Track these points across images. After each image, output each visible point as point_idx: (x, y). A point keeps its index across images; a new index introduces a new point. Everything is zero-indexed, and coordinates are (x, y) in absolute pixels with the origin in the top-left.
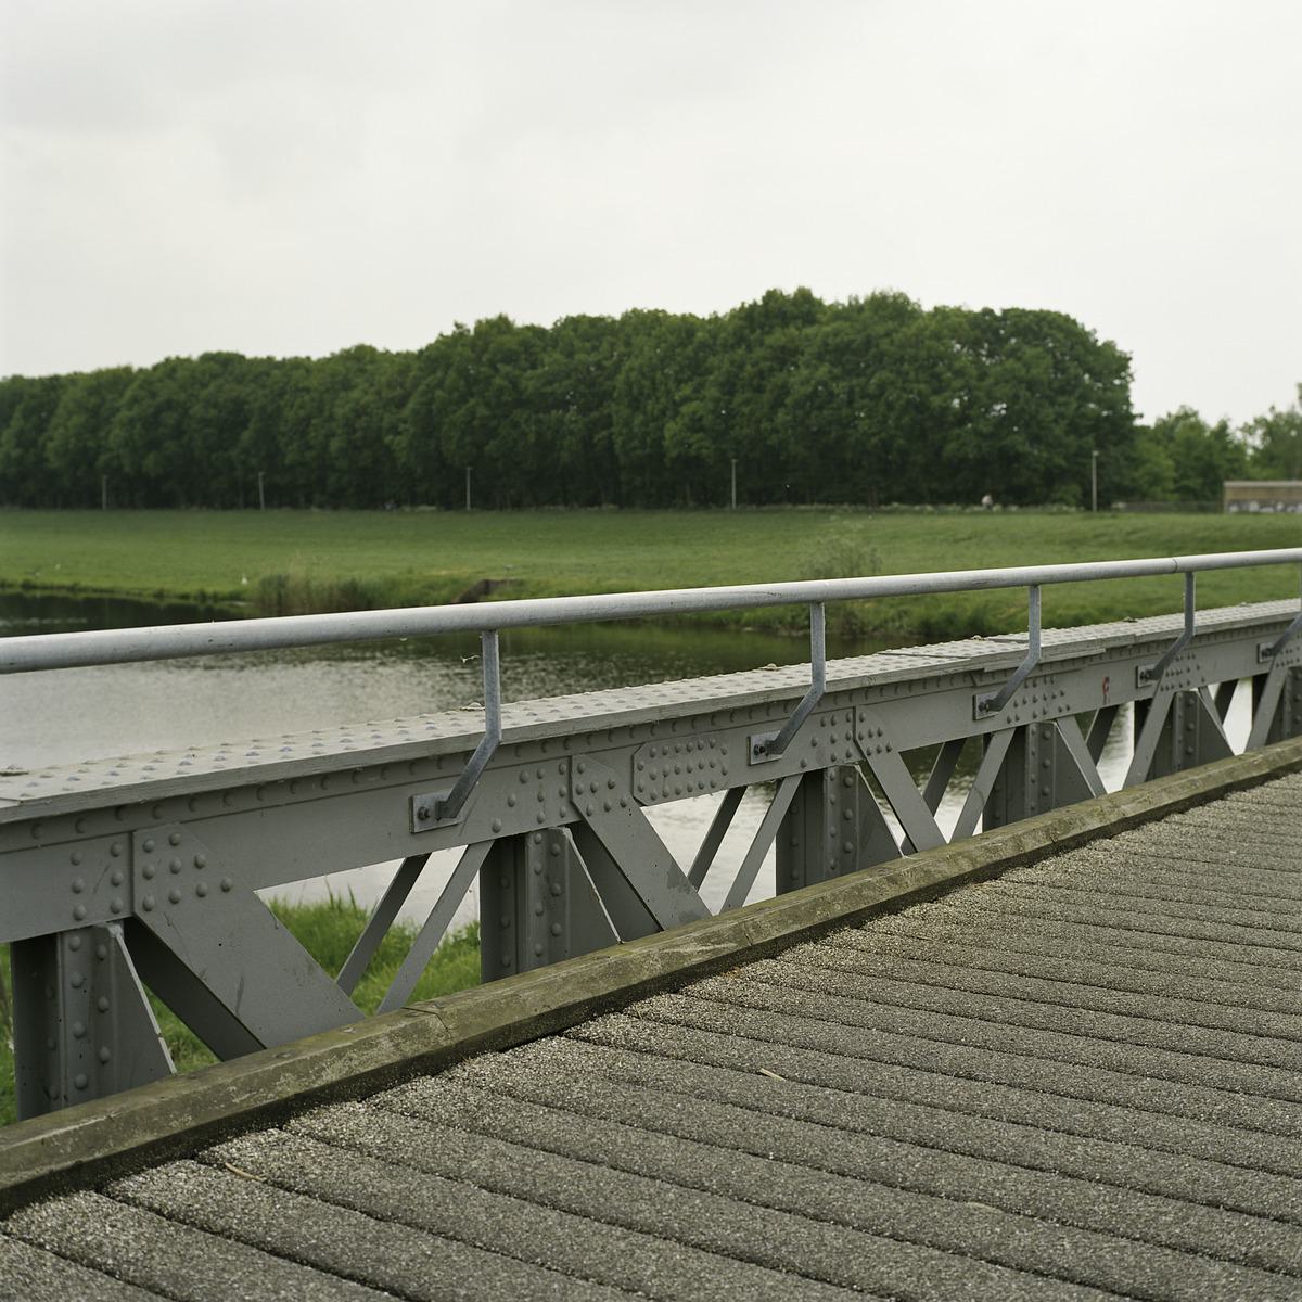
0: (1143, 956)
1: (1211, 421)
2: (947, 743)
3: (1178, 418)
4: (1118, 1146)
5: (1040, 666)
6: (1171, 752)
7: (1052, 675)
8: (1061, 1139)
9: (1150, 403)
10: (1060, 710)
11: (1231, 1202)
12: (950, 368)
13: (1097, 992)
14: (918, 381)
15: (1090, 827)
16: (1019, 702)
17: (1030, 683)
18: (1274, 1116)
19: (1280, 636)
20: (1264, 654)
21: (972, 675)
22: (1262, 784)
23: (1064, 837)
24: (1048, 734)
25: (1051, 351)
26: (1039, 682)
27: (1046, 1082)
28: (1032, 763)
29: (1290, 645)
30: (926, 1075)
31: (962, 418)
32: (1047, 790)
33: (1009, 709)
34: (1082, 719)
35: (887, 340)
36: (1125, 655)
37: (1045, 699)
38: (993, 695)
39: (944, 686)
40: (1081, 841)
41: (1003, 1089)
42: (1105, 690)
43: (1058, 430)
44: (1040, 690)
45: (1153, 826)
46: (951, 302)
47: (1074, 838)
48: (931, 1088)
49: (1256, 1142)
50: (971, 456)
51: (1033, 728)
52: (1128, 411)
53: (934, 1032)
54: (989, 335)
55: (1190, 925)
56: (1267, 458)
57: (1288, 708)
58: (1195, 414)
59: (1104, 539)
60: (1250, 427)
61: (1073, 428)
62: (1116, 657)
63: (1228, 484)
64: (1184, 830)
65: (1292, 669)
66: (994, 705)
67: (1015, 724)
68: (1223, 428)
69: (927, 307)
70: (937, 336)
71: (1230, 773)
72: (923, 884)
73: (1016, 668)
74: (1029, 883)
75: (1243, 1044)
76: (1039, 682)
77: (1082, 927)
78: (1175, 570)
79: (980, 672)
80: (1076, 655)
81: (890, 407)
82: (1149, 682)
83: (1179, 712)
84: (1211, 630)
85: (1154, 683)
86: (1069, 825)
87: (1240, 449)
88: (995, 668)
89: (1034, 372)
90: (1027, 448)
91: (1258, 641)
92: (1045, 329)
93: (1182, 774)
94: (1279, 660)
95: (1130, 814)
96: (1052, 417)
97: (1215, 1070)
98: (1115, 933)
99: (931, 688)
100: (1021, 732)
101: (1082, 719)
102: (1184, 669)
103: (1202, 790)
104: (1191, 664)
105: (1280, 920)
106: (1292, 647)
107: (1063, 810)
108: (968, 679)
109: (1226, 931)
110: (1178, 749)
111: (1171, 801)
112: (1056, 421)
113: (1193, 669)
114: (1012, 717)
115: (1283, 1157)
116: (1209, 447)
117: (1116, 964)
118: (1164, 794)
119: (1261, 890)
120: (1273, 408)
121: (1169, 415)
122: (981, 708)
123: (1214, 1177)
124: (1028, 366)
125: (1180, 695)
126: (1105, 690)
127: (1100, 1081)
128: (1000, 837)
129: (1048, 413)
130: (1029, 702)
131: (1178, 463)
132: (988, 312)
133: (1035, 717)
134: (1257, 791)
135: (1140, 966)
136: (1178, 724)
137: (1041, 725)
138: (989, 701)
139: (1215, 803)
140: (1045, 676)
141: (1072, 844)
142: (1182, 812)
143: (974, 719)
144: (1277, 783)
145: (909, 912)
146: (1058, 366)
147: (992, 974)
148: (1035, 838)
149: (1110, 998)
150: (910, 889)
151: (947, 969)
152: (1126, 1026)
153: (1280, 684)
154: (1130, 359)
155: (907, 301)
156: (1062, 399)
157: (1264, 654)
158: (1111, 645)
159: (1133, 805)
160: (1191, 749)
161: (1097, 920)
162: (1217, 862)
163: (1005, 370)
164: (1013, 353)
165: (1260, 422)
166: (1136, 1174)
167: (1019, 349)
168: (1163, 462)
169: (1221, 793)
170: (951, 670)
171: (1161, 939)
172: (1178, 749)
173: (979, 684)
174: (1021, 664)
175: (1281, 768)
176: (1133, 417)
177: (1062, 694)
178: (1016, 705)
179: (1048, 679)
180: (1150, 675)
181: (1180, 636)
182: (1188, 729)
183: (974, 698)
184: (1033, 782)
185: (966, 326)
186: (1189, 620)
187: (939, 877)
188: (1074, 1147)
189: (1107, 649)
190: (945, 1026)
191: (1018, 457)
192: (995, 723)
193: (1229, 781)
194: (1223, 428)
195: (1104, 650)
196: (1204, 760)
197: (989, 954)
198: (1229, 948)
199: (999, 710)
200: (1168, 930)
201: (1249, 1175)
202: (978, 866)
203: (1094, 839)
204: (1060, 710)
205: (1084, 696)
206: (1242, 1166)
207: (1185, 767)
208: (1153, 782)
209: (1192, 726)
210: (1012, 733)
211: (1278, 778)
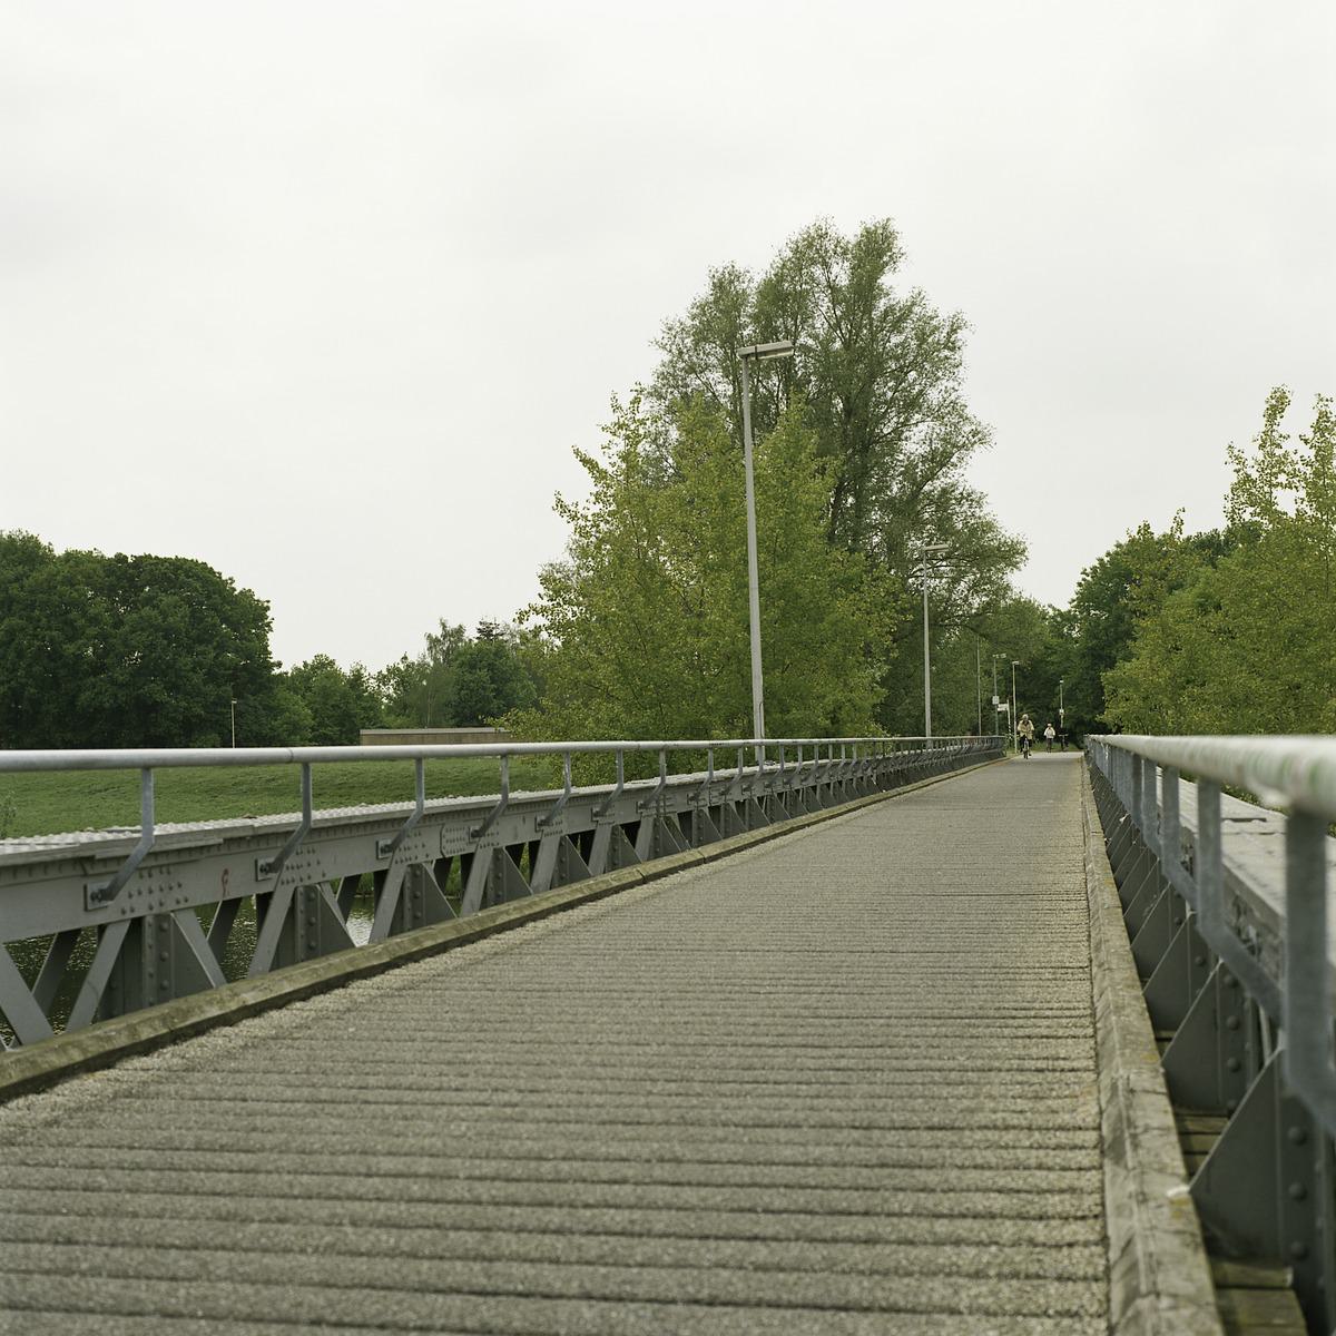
0: (258, 1121)
1: (345, 667)
2: (60, 934)
3: (313, 668)
4: (223, 1285)
5: (155, 855)
6: (294, 947)
7: (168, 865)
8: (164, 1286)
9: (288, 650)
10: (178, 902)
11: (334, 1318)
12: (84, 613)
13: (209, 1155)
14: (50, 628)
15: (209, 1015)
16: (135, 893)
17: (145, 873)
18: (379, 1241)
19: (396, 834)
20: (383, 851)
21: (81, 862)
22: (383, 973)
23: (182, 1025)
24: (165, 926)
25: (189, 601)
26: (155, 872)
27: (150, 1238)
28: (149, 956)
29: (406, 842)
30: (21, 1246)
31: (98, 668)
32: (166, 983)
33: (122, 899)
34: (203, 911)
35: (16, 585)
36: (244, 848)
37: (161, 890)
38: (105, 884)
39: (53, 873)
40: (200, 1029)
41: (105, 1249)
42: (225, 882)
43: (197, 679)
44: (157, 881)
45: (274, 1014)
46: (83, 546)
47: (193, 1026)
48: (27, 1256)
49: (361, 1265)
50: (107, 705)
51: (149, 920)
52: (265, 660)
53: (32, 1206)
54: (125, 583)
55: (306, 1092)
56: (401, 707)
57: (408, 904)
58: (332, 663)
59: (244, 787)
60: (385, 677)
61: (211, 677)
62: (234, 849)
63: (363, 732)
64: (305, 1014)
65: (411, 866)
66: (106, 895)
67: (130, 916)
68: (357, 677)
69: (59, 551)
70: (70, 582)
71: (351, 961)
72: (28, 1074)
73: (127, 857)
74: (143, 1070)
75: (352, 1185)
76: (155, 872)
77: (197, 1103)
78: (291, 760)
79: (91, 859)
80: (193, 844)
81: (20, 654)
82: (270, 875)
83: (300, 906)
84: (330, 824)
85: (273, 876)
86: (187, 1013)
87: (374, 698)
88: (110, 855)
89: (171, 619)
90: (164, 697)
91: (377, 838)
92: (182, 577)
93: (305, 964)
94: (398, 855)
95: (251, 1002)
96: (190, 666)
97: (322, 1210)
98: (231, 1104)
99: (39, 875)
100: (137, 923)
101: (203, 911)
102: (305, 864)
103: (323, 979)
104: (312, 858)
105: (394, 1081)
106: (410, 844)
107: (182, 1000)
108: (78, 867)
109: (342, 1093)
110: (300, 943)
111: (291, 989)
112: (193, 670)
113: (314, 864)
114: (128, 909)
115: (386, 1274)
116: (344, 695)
117: (230, 1130)
118: (285, 983)
119: (378, 1058)
120: (405, 658)
121: (306, 664)
122: (93, 899)
123: (317, 1299)
124: (164, 615)
125: (301, 889)
126: (225, 882)
127: (207, 1232)
128: (113, 1027)
129: (186, 661)
130: (145, 892)
131: (316, 711)
132: (121, 558)
133: (151, 908)
134: (377, 979)
135: (254, 1129)
136: (300, 917)
137: (158, 917)
138: (101, 891)
139: (337, 991)
140: (161, 866)
141: (191, 1032)
142: (304, 1000)
143: (86, 909)
144: (397, 971)
145: (13, 1104)
146: (196, 617)
147: (100, 1151)
148: (151, 1026)
149: (224, 1159)
150: (14, 1080)
151: (52, 1150)
152: (237, 1181)
153: (400, 881)
154: (268, 608)
155: (37, 544)
156: (200, 648)
157: (383, 851)
158: (229, 835)
159: (252, 993)
160: (313, 944)
161: (213, 1095)
162: (335, 1038)
163: (141, 617)
164: (149, 601)
165: (393, 671)
166: (239, 1306)
167: (154, 598)
168: (303, 711)
169: (342, 981)
170: (59, 856)
171: (277, 1106)
172: (300, 943)
173: (91, 872)
174: (132, 851)
175: (401, 957)
176: (271, 666)
177: (180, 886)
178: (130, 896)
179: (164, 869)
180: (269, 868)
181: (297, 829)
182: (310, 924)
183: (85, 888)
184: (151, 976)
185: (101, 573)
186: (307, 816)
187: (46, 1067)
188: (177, 1290)
189: (225, 840)
190: (45, 1200)
191: (156, 706)
192: (109, 913)
193: (350, 969)
194: (357, 677)
195: (221, 840)
196: (327, 951)
197: (96, 1132)
198: (343, 1107)
199: (112, 899)
200: (284, 1097)
201: (354, 1294)
202: (89, 1055)
203: (214, 1027)
204: (178, 902)
205: (204, 887)
206: (347, 1287)
207: (308, 958)
208: (275, 973)
209: (313, 920)
210: (127, 925)
211: (399, 967)
